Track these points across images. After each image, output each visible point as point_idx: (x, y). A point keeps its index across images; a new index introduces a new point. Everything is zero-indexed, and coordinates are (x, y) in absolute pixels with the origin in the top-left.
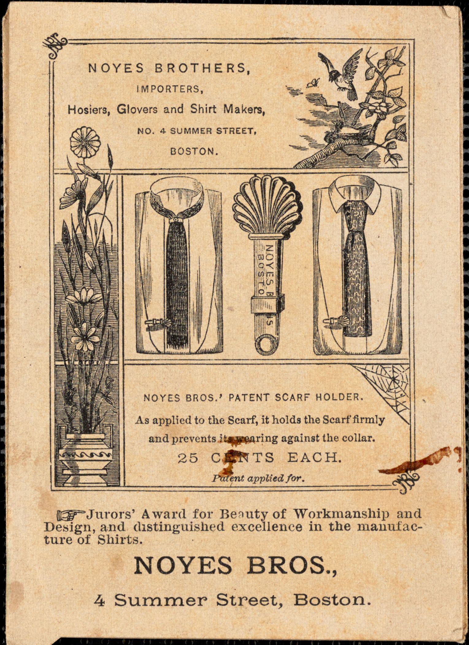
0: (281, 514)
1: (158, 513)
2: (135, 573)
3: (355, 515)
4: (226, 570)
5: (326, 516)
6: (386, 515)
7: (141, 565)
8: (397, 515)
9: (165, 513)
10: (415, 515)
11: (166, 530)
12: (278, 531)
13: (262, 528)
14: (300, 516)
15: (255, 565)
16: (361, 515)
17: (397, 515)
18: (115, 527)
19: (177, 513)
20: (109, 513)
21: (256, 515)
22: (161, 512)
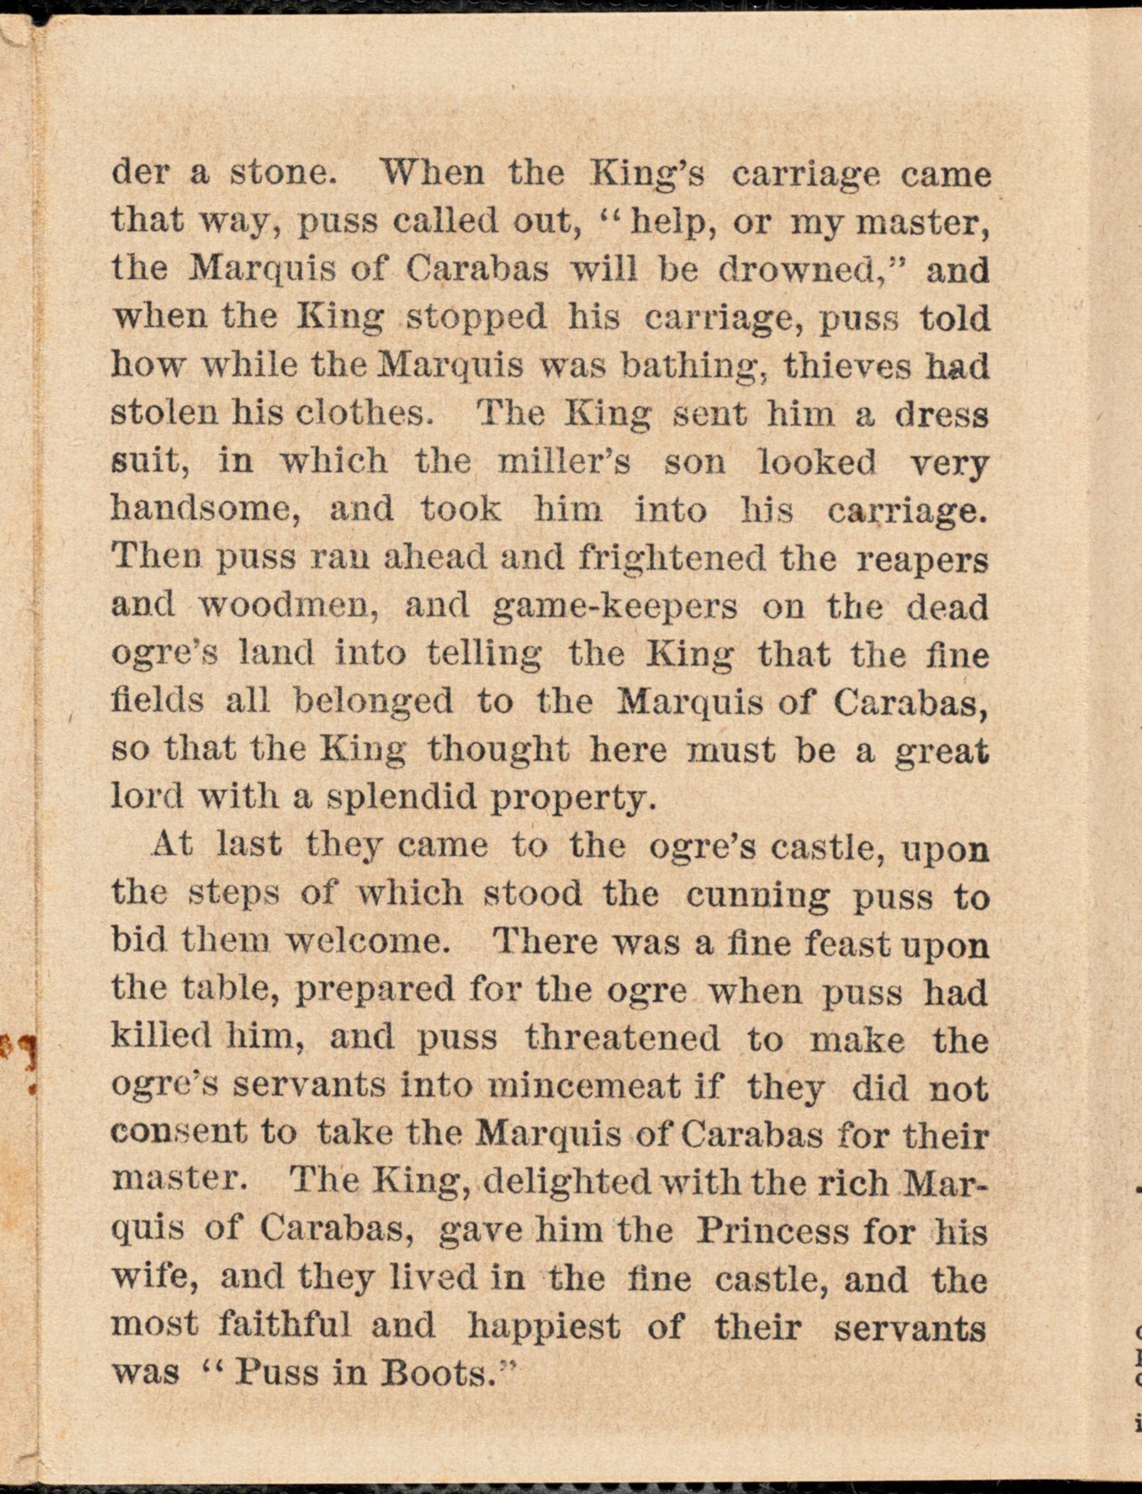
0: (323, 893)
1: (127, 1367)
3: (352, 1377)
5: (611, 613)
6: (905, 416)
9: (147, 1369)
10: (235, 557)
14: (399, 178)
16: (867, 996)
19: (576, 937)
20: (871, 555)
21: (672, 1089)
22: (137, 1367)
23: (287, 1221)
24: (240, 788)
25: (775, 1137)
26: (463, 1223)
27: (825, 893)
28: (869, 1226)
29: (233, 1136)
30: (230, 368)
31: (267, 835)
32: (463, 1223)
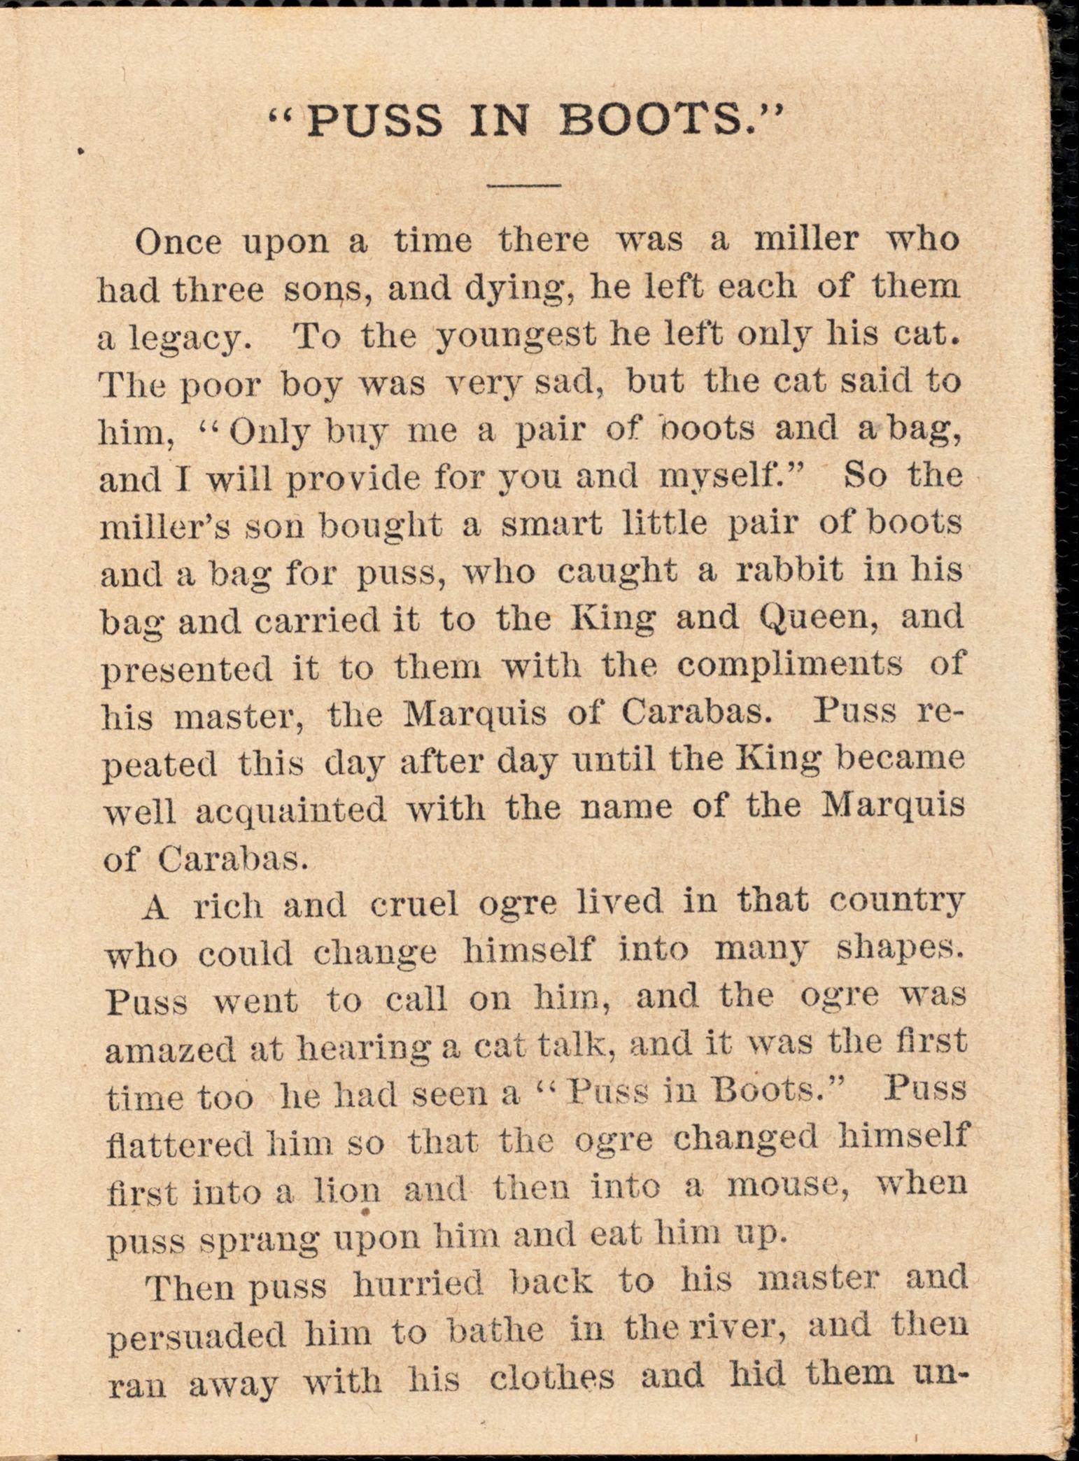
2: (310, 134)
4: (430, 128)
7: (506, 120)
8: (390, 291)
11: (637, 958)
12: (194, 681)
13: (750, 479)
15: (575, 119)
17: (390, 291)
18: (320, 907)
23: (648, 705)
24: (447, 801)
25: (715, 714)
26: (685, 706)
27: (650, 615)
28: (440, 472)
29: (653, 954)
30: (904, 1186)
31: (829, 1268)
32: (685, 706)
